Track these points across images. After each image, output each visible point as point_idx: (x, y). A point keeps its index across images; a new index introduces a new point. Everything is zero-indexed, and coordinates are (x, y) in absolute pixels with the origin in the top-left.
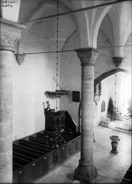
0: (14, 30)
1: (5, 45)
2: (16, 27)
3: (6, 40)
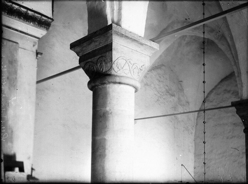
0: (138, 49)
1: (124, 75)
2: (142, 44)
3: (126, 67)
